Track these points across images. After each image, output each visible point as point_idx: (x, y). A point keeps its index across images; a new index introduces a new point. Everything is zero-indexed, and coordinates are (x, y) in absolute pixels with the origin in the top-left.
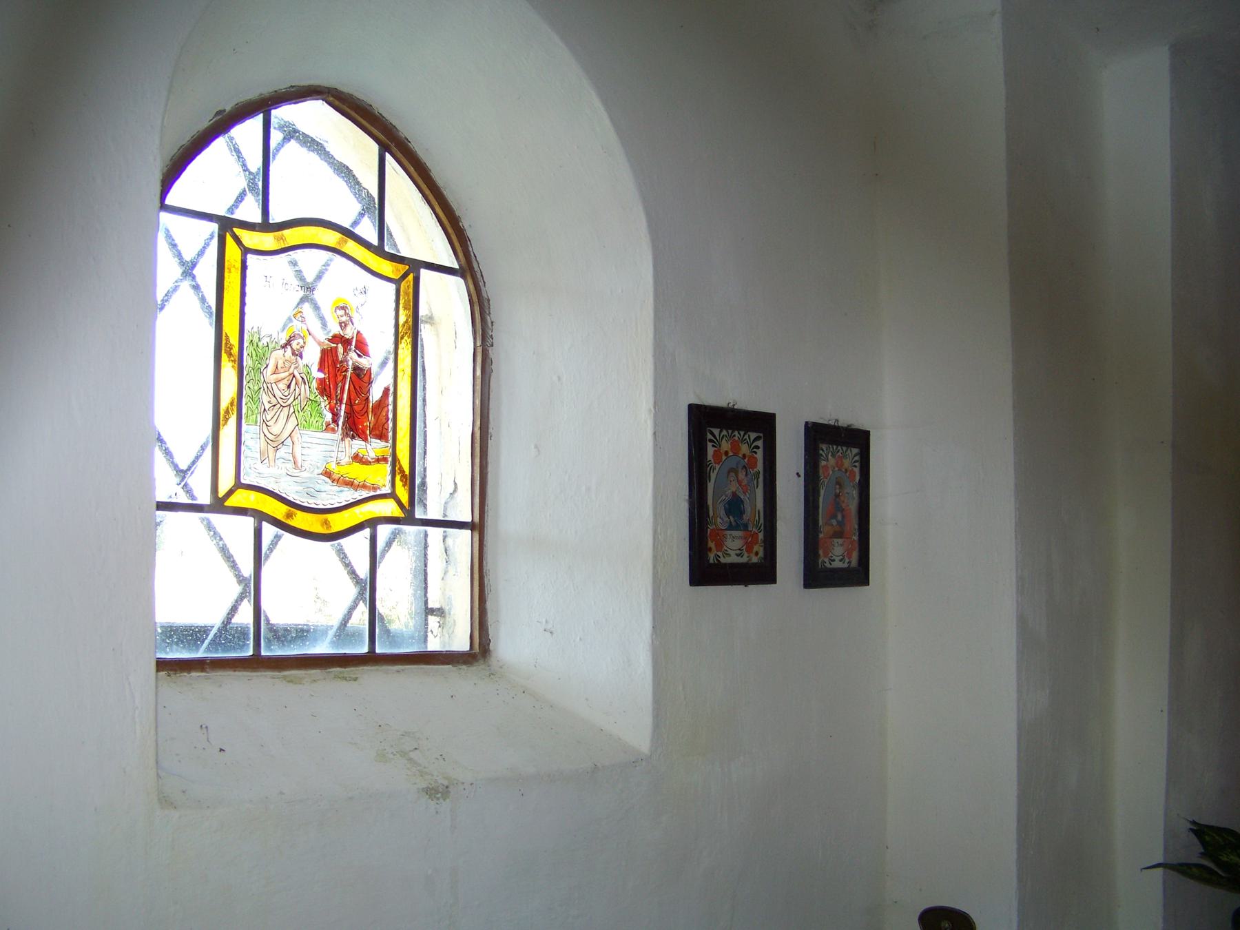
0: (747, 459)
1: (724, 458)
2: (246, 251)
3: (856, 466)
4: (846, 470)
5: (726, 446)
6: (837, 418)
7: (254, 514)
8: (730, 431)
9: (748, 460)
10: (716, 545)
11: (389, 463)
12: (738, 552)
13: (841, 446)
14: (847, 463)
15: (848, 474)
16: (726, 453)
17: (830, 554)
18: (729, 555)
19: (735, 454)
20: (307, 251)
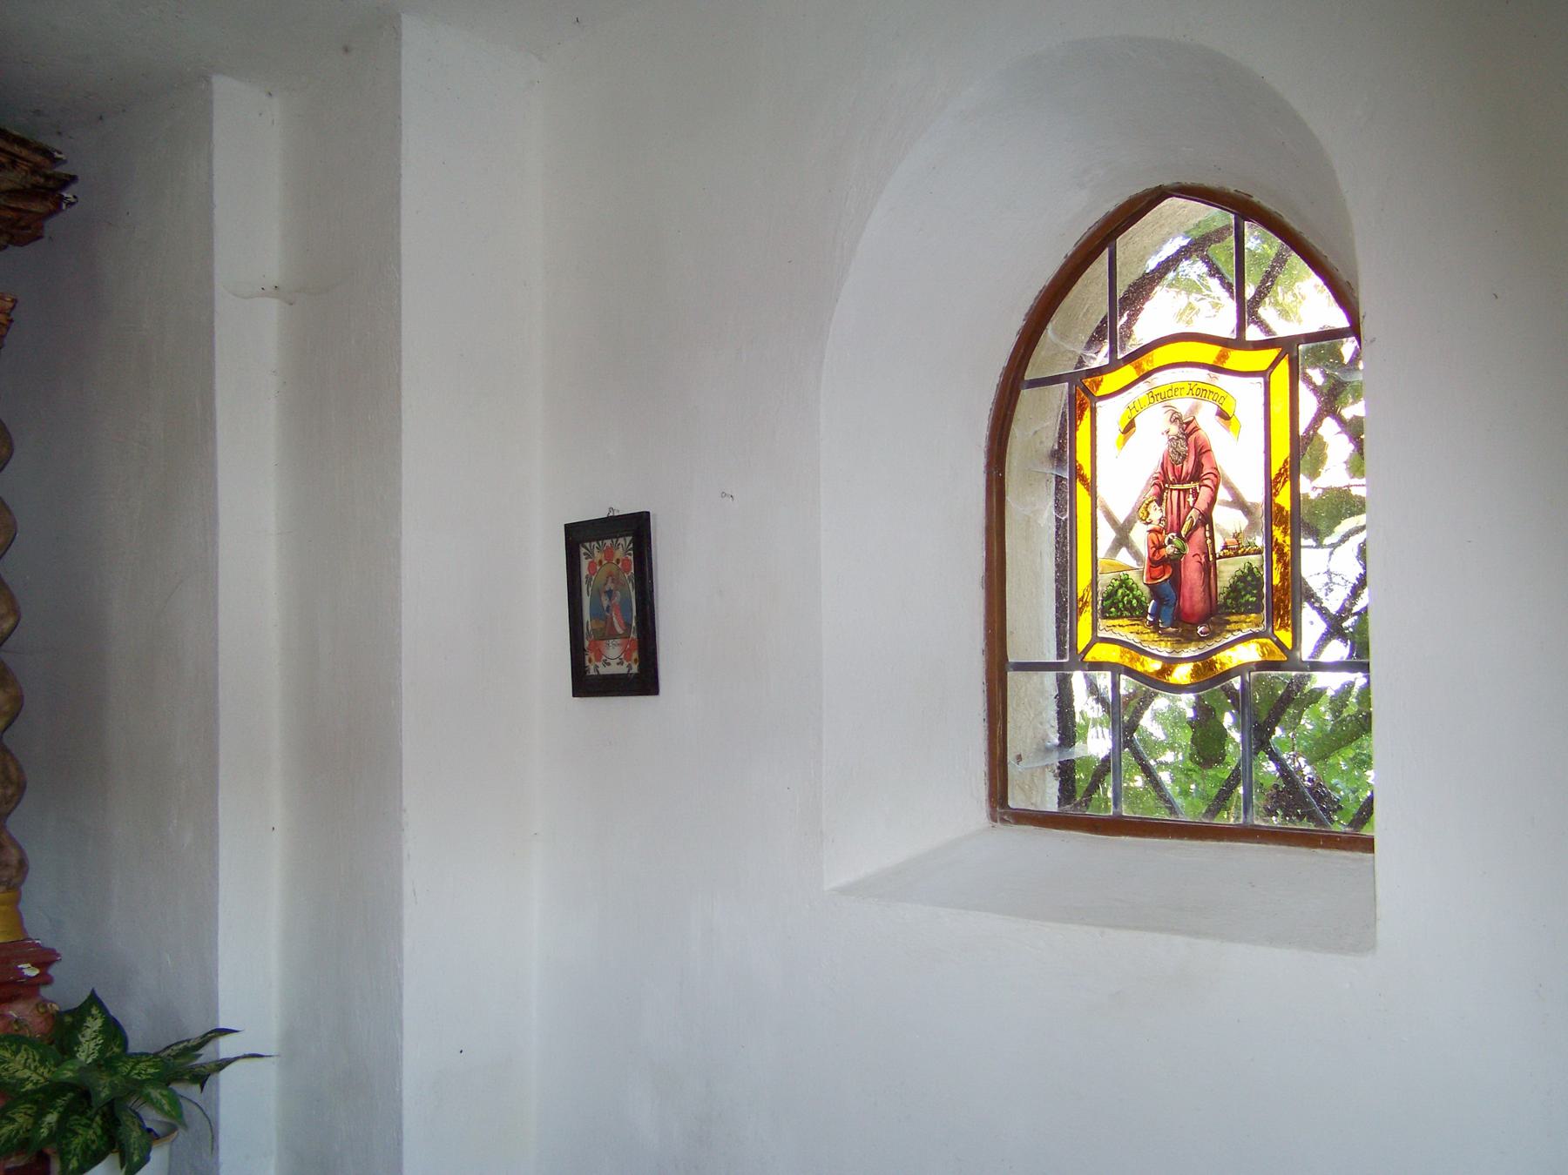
0: (620, 564)
1: (598, 568)
2: (1265, 374)
3: (630, 554)
4: (618, 561)
5: (598, 556)
6: (609, 506)
7: (1304, 665)
8: (615, 540)
9: (622, 565)
10: (595, 656)
11: (1188, 587)
12: (618, 660)
13: (597, 541)
14: (619, 554)
15: (620, 565)
16: (600, 562)
17: (604, 658)
18: (609, 664)
19: (609, 561)
20: (1119, 388)
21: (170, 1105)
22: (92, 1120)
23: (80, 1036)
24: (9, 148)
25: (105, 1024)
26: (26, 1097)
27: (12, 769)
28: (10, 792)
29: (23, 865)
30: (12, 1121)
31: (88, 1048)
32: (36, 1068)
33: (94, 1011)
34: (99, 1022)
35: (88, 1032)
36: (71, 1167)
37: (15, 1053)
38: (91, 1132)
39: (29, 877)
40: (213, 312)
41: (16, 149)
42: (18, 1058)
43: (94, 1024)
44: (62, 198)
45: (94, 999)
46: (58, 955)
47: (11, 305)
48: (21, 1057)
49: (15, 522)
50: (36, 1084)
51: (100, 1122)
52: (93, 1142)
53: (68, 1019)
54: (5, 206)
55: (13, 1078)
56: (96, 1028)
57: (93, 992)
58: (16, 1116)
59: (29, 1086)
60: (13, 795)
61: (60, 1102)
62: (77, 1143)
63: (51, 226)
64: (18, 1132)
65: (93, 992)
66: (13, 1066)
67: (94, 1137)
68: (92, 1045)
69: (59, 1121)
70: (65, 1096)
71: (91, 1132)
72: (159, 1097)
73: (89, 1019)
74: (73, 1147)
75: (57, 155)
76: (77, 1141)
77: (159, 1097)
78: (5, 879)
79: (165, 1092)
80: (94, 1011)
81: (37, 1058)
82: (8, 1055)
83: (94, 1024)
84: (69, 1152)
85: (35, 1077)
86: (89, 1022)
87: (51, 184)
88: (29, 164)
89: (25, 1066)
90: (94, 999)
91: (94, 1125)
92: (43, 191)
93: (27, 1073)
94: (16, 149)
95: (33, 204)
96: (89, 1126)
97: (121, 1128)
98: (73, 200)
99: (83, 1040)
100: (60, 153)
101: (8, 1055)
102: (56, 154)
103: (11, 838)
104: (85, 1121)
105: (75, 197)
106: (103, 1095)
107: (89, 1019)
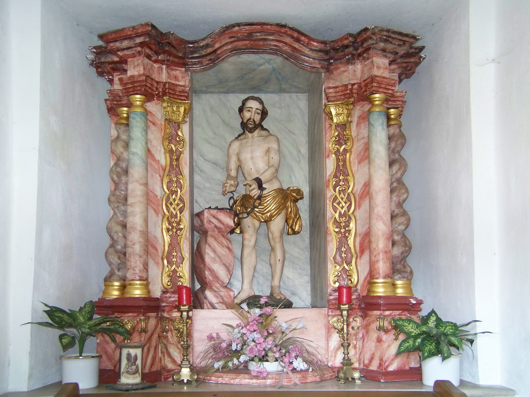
21: (458, 342)
22: (432, 343)
23: (429, 322)
24: (403, 39)
25: (436, 319)
26: (413, 336)
27: (407, 242)
28: (407, 249)
29: (411, 272)
30: (409, 342)
31: (432, 323)
32: (415, 329)
33: (433, 315)
34: (435, 318)
35: (431, 321)
36: (425, 355)
37: (409, 324)
38: (432, 346)
39: (414, 276)
40: (469, 73)
41: (405, 39)
42: (410, 325)
43: (433, 318)
44: (421, 57)
45: (433, 311)
46: (423, 301)
47: (405, 94)
48: (411, 325)
49: (407, 163)
50: (415, 333)
51: (435, 345)
52: (432, 349)
53: (425, 318)
54: (403, 62)
55: (409, 331)
56: (434, 320)
57: (433, 309)
58: (409, 341)
59: (413, 334)
60: (408, 250)
61: (422, 337)
62: (427, 349)
63: (418, 69)
64: (410, 346)
65: (433, 309)
66: (408, 328)
67: (432, 348)
68: (433, 324)
69: (421, 341)
70: (423, 335)
71: (432, 346)
72: (454, 340)
73: (431, 317)
74: (426, 349)
75: (418, 37)
76: (427, 348)
77: (454, 340)
78: (406, 276)
79: (456, 339)
80: (433, 315)
81: (415, 326)
82: (407, 324)
83: (433, 318)
84: (425, 351)
85: (415, 332)
86: (432, 317)
87: (417, 51)
88: (409, 43)
89: (412, 328)
90: (433, 311)
91: (433, 345)
92: (414, 54)
93: (413, 330)
94: (405, 39)
95: (411, 59)
96: (431, 345)
97: (399, 72)
98: (424, 57)
99: (429, 323)
100: (418, 36)
101: (407, 324)
102: (417, 37)
103: (408, 265)
104: (429, 343)
105: (425, 56)
106: (434, 333)
107: (431, 317)
